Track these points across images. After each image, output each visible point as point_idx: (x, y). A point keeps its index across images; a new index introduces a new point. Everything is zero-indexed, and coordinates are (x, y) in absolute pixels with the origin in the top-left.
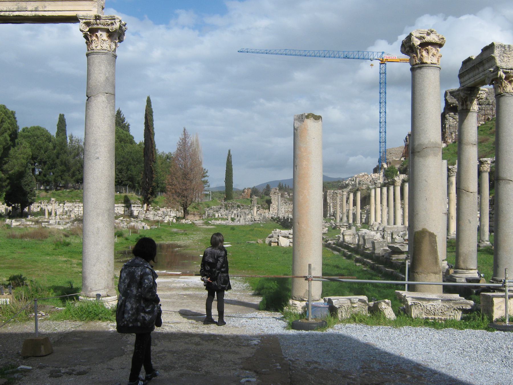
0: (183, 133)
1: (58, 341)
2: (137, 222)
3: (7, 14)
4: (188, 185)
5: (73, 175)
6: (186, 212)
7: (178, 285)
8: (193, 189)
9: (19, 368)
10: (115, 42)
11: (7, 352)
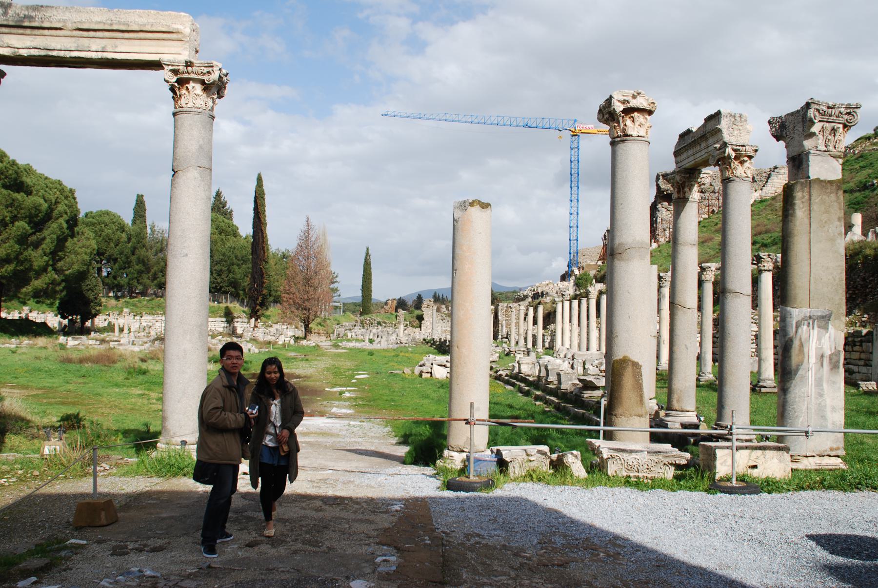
0: (305, 223)
3: (62, 54)
4: (311, 293)
6: (308, 331)
8: (318, 299)
9: (68, 542)
10: (213, 98)
11: (52, 521)
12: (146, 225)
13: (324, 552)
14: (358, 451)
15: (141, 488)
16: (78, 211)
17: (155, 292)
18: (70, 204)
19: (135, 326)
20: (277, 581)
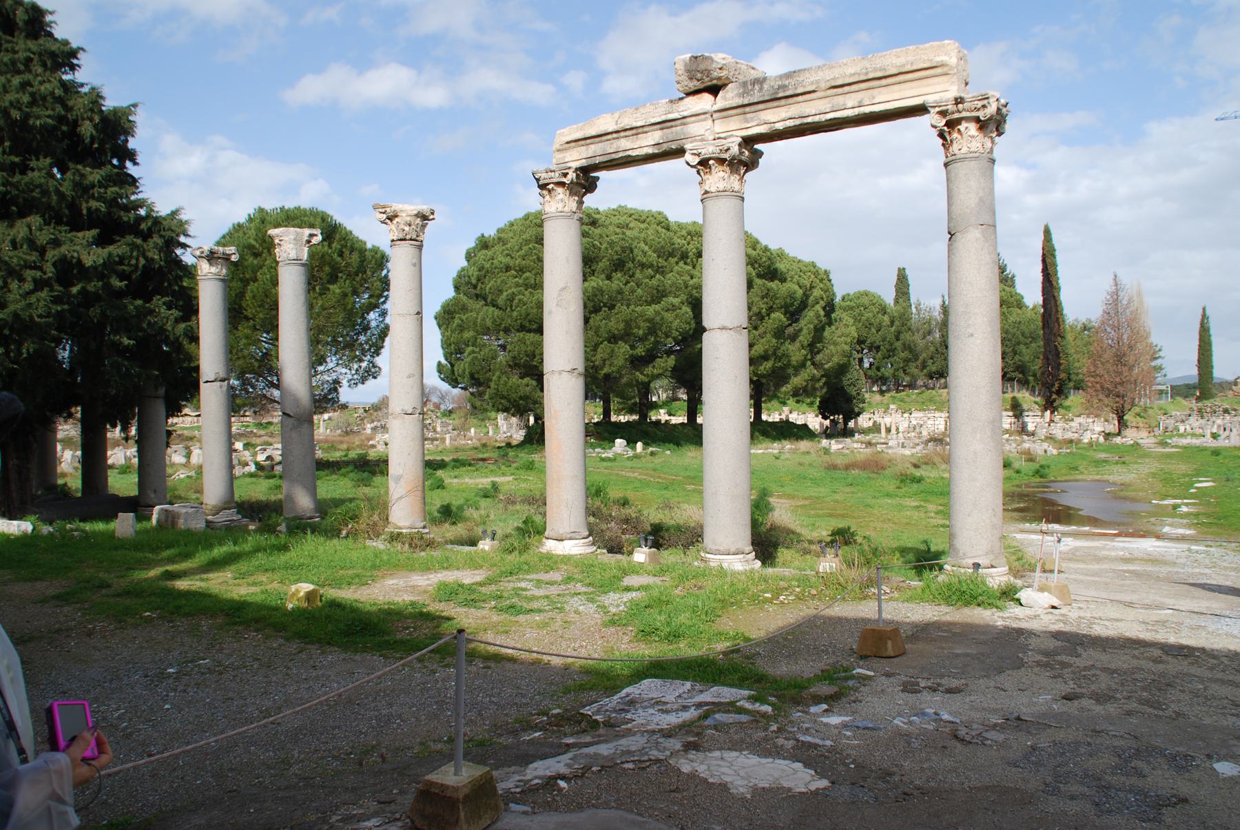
0: (1112, 282)
1: (913, 635)
2: (1034, 442)
3: (817, 119)
4: (1125, 375)
5: (924, 366)
6: (1122, 424)
7: (1113, 554)
8: (1135, 381)
9: (854, 672)
10: (991, 137)
11: (835, 646)
12: (910, 303)
13: (1170, 717)
14: (1207, 586)
15: (928, 616)
16: (834, 294)
17: (924, 383)
18: (825, 288)
19: (903, 426)
20: (1107, 748)
